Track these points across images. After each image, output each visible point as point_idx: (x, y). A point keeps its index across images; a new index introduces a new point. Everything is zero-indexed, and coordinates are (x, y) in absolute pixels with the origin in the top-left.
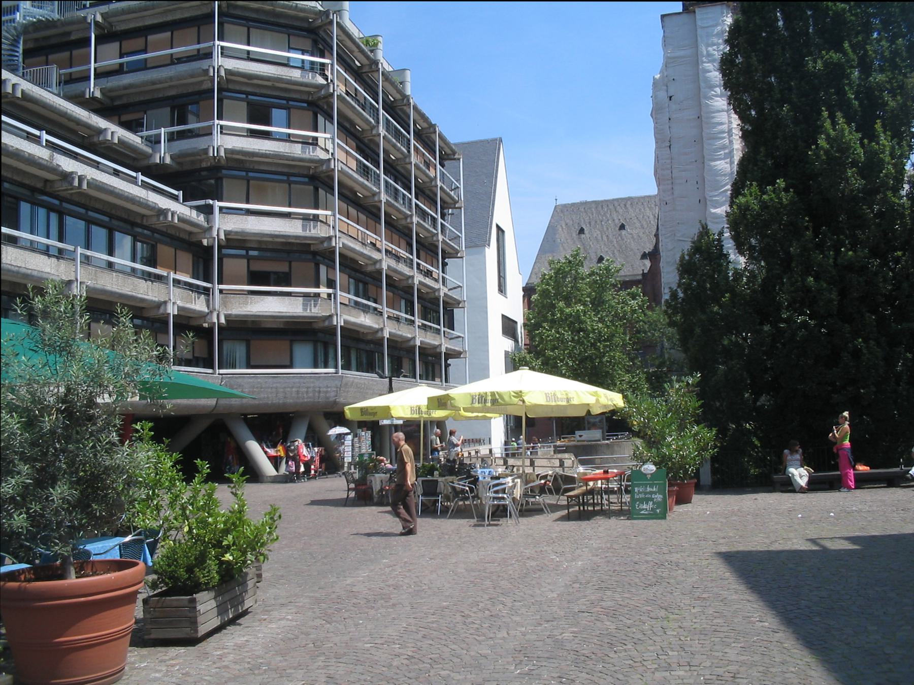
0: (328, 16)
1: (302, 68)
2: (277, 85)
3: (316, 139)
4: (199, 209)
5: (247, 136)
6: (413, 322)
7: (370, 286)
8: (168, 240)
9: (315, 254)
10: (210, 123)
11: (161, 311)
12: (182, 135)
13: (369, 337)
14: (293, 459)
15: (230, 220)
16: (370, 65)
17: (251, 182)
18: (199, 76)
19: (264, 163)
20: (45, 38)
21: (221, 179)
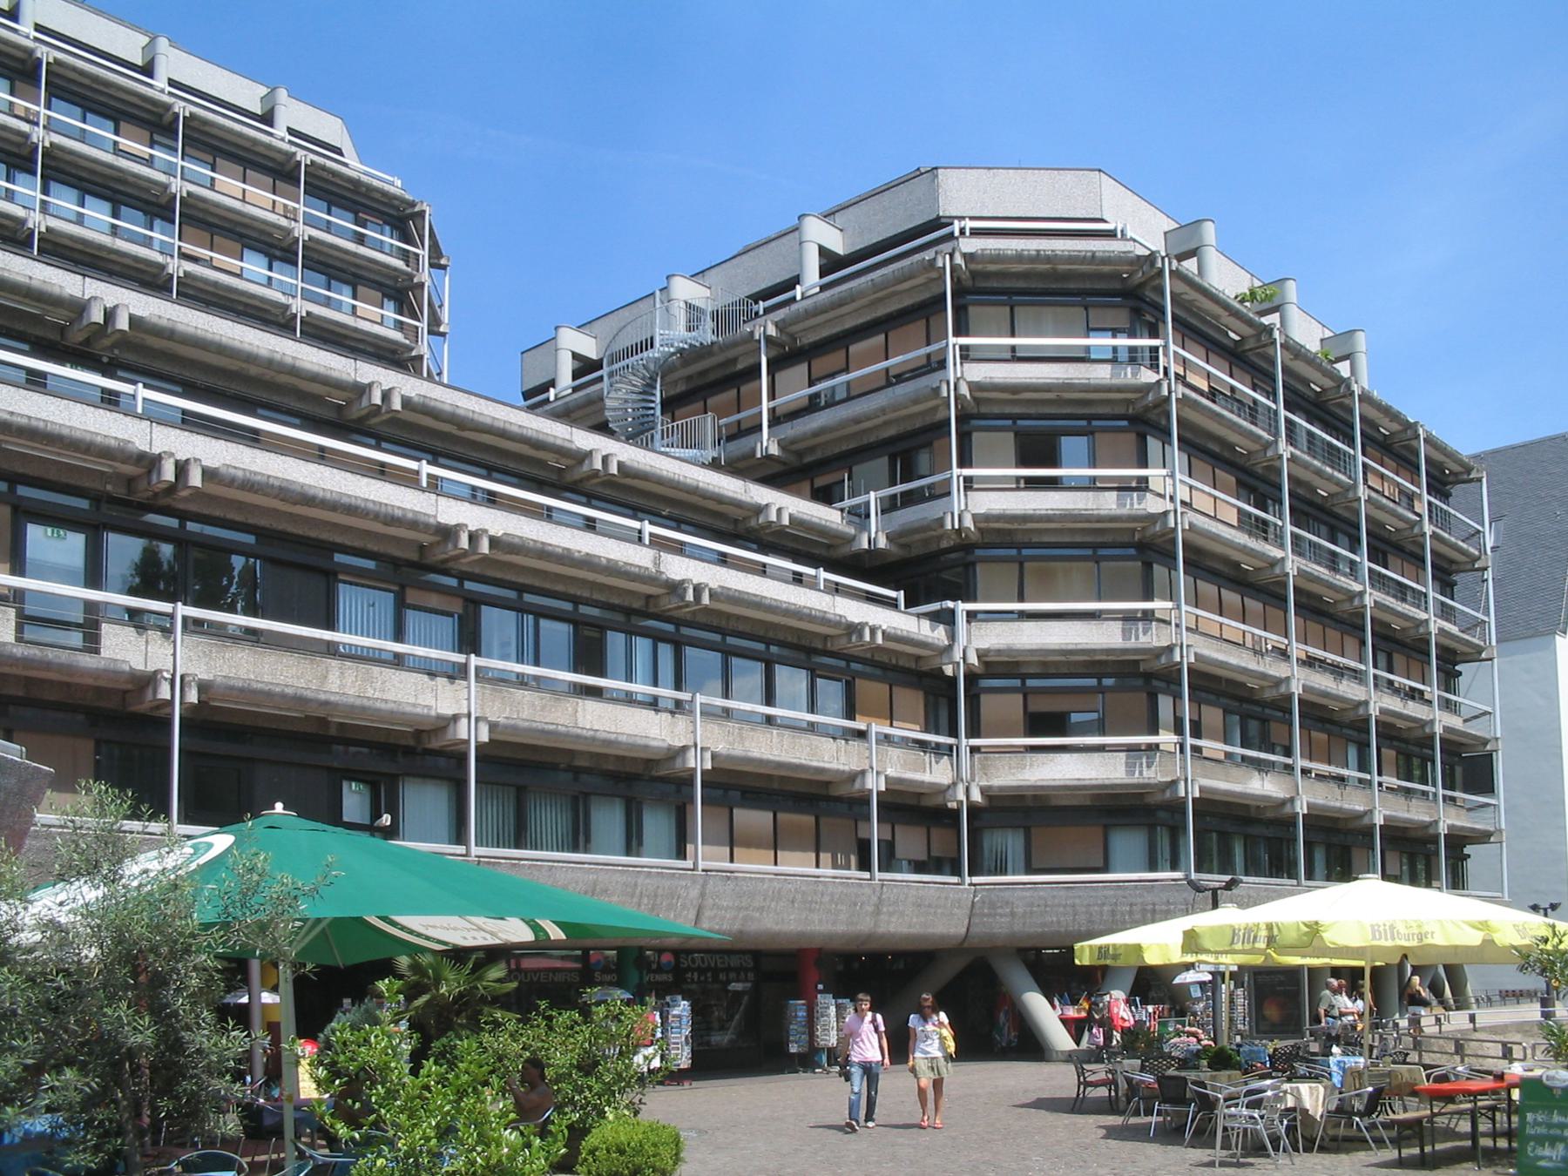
0: (1153, 263)
1: (1114, 361)
2: (1067, 396)
3: (1145, 479)
4: (935, 617)
5: (1018, 489)
6: (1370, 783)
7: (1273, 725)
8: (878, 672)
9: (1148, 676)
10: (946, 475)
11: (857, 785)
12: (909, 499)
13: (1270, 815)
14: (1101, 1024)
15: (984, 632)
16: (1258, 336)
17: (1027, 565)
18: (926, 399)
19: (1047, 530)
20: (703, 373)
21: (973, 564)
